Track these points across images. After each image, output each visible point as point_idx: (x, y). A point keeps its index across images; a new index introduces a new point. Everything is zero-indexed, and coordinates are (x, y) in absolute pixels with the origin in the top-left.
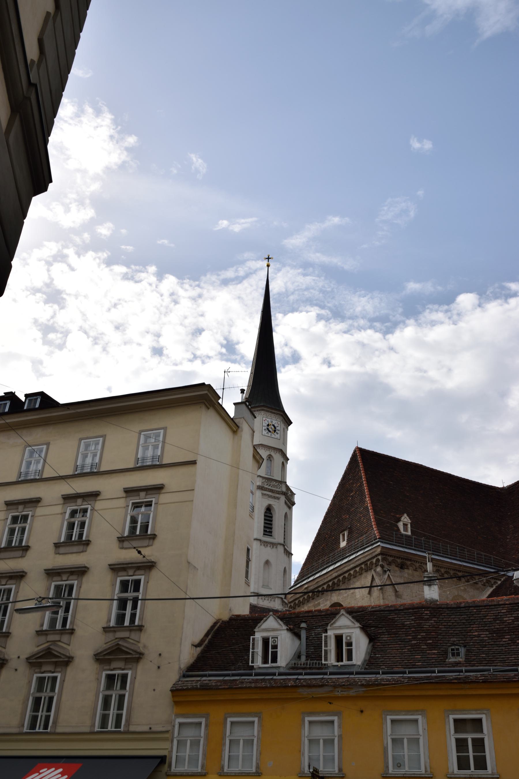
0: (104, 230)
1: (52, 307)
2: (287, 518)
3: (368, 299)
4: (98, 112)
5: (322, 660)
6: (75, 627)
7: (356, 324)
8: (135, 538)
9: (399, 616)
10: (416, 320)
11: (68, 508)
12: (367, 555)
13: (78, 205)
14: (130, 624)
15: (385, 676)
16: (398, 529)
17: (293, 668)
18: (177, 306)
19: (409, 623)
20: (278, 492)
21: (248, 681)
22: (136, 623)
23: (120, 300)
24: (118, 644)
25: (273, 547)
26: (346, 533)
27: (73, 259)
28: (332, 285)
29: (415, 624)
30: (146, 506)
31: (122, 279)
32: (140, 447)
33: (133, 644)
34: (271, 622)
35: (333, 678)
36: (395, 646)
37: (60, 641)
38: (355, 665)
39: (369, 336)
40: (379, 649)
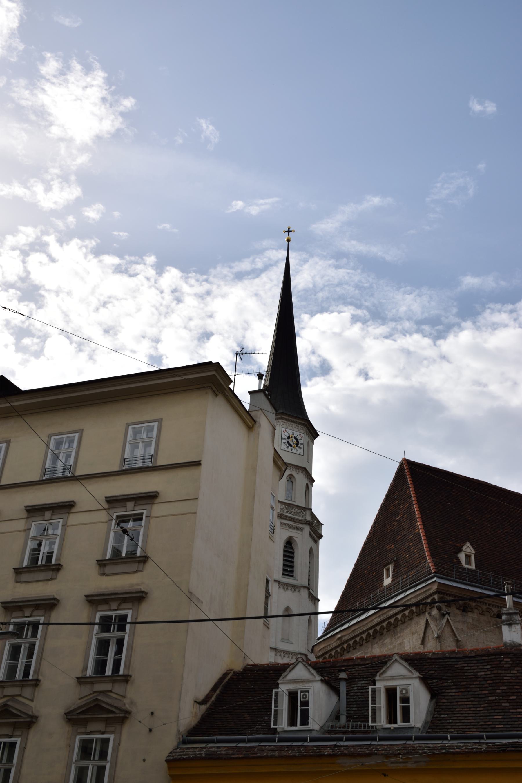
0: (93, 213)
1: (27, 306)
2: (313, 555)
3: (415, 296)
4: (88, 69)
5: (368, 721)
6: (40, 678)
7: (399, 327)
8: (120, 561)
9: (470, 665)
10: (474, 323)
11: (34, 523)
12: (419, 595)
13: (61, 182)
14: (112, 673)
15: (455, 742)
16: (459, 562)
17: (329, 732)
18: (181, 305)
19: (483, 673)
20: (301, 522)
21: (270, 748)
22: (121, 672)
23: (110, 297)
24: (97, 700)
25: (295, 590)
26: (391, 567)
27: (54, 248)
28: (371, 280)
29: (492, 675)
30: (135, 520)
31: (113, 272)
32: (127, 444)
33: (116, 699)
34: (300, 672)
35: (385, 745)
36: (466, 703)
37: (20, 695)
38: (413, 728)
39: (417, 342)
40: (444, 707)
